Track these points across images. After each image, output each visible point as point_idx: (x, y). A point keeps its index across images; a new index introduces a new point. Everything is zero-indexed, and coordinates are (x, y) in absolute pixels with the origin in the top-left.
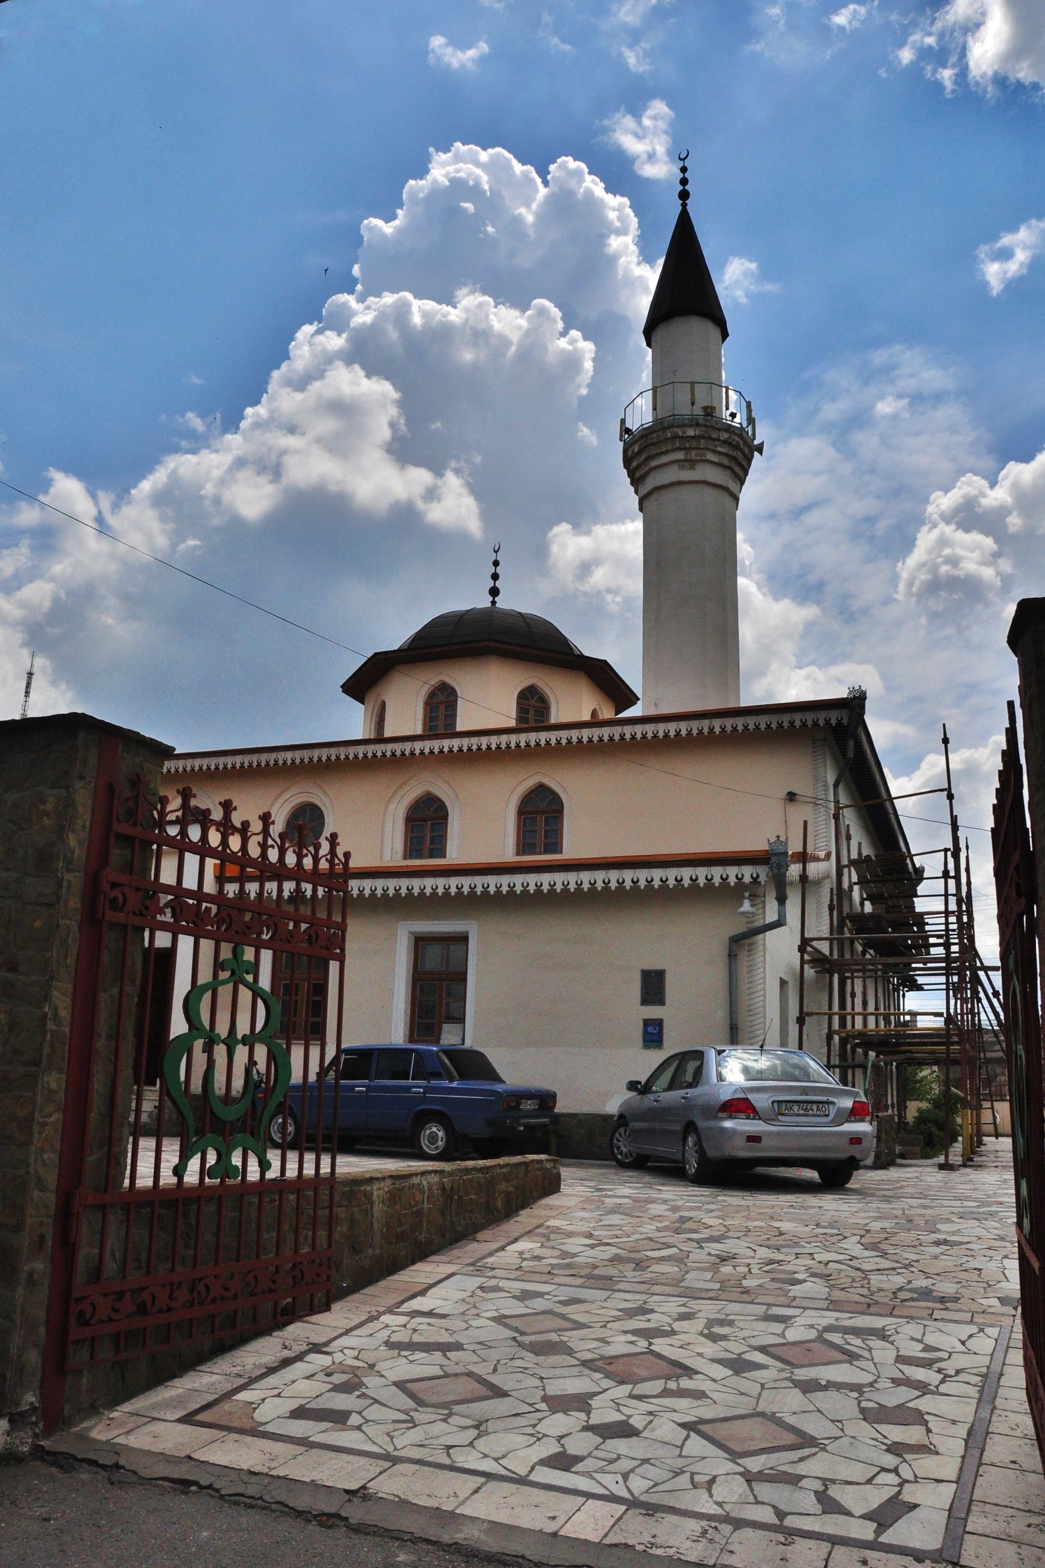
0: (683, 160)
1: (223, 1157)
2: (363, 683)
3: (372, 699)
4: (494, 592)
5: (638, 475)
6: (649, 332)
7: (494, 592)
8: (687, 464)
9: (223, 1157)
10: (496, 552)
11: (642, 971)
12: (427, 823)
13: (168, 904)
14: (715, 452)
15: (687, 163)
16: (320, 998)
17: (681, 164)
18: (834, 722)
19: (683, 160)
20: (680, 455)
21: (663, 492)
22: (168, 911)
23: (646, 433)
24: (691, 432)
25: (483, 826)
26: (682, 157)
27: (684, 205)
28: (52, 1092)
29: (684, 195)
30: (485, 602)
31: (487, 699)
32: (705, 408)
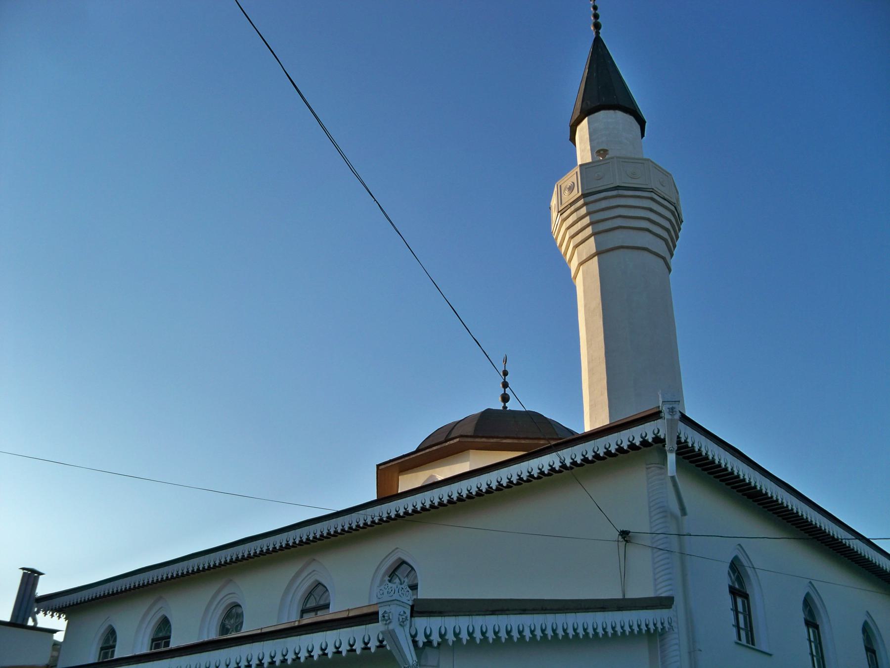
4: (505, 398)
7: (505, 398)
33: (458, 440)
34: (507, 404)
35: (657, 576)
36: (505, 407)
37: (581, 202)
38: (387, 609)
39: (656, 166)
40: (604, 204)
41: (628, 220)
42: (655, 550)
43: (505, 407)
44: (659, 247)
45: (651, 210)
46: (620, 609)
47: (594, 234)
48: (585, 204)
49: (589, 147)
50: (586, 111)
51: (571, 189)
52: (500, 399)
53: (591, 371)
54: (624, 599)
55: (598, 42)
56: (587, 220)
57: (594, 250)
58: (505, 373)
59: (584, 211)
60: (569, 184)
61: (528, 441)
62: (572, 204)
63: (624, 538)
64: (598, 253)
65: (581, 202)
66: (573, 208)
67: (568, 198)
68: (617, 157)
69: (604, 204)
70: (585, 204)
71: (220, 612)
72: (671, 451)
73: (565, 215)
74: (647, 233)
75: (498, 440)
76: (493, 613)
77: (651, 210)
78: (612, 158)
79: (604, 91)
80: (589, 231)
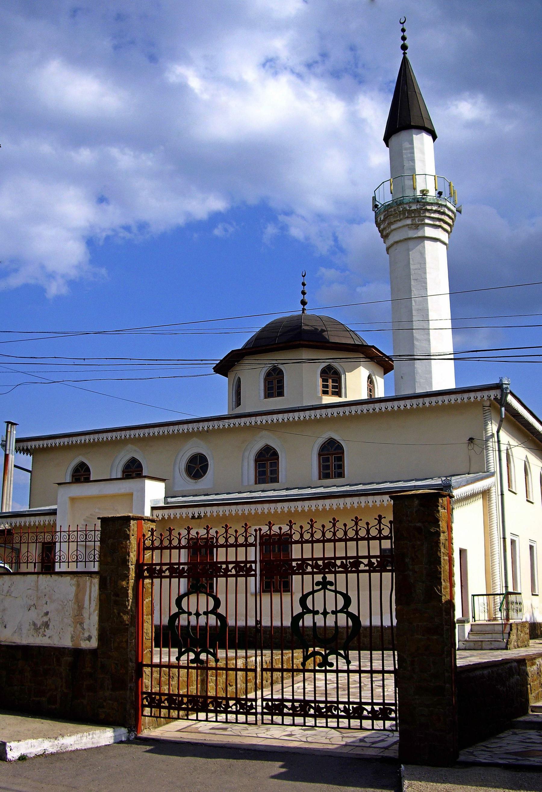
0: (403, 23)
1: (197, 655)
2: (224, 367)
3: (232, 374)
5: (385, 233)
6: (387, 139)
8: (413, 226)
9: (197, 655)
10: (304, 276)
13: (166, 699)
14: (430, 218)
15: (405, 26)
16: (274, 476)
17: (401, 27)
19: (403, 23)
20: (409, 222)
21: (399, 244)
22: (166, 702)
23: (388, 207)
24: (414, 207)
26: (402, 22)
27: (404, 54)
28: (133, 633)
29: (404, 47)
30: (296, 310)
32: (422, 191)
55: (405, 62)
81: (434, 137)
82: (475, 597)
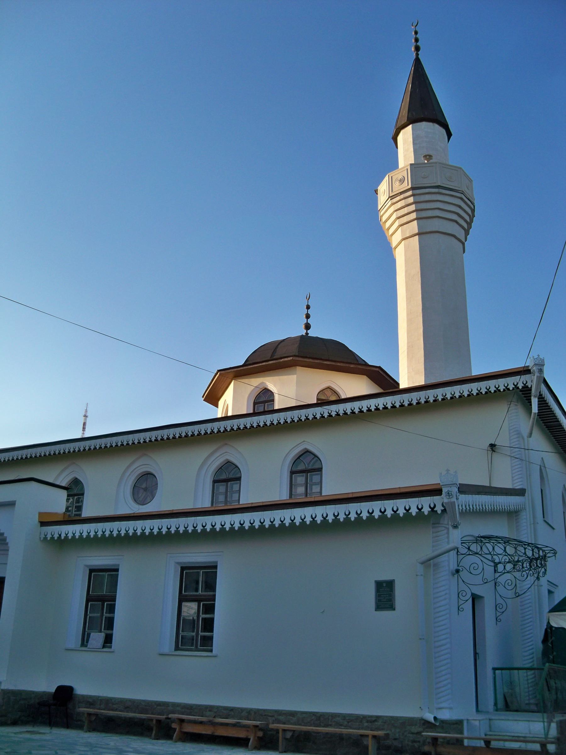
4: (308, 327)
7: (308, 327)
11: (394, 610)
12: (227, 477)
18: (520, 386)
25: (265, 473)
30: (304, 332)
31: (289, 389)
33: (291, 358)
34: (309, 331)
35: (514, 471)
36: (307, 334)
37: (410, 193)
38: (450, 489)
39: (465, 174)
40: (427, 197)
41: (446, 213)
42: (513, 458)
43: (307, 334)
44: (460, 234)
45: (460, 207)
46: (486, 493)
47: (417, 219)
48: (413, 195)
49: (412, 149)
50: (412, 121)
51: (402, 181)
52: (304, 326)
53: (410, 321)
54: (490, 487)
55: (418, 63)
56: (413, 207)
57: (416, 231)
58: (308, 307)
59: (411, 200)
60: (400, 177)
61: (342, 364)
62: (401, 193)
63: (492, 449)
64: (419, 234)
65: (410, 193)
66: (402, 196)
67: (398, 188)
68: (440, 163)
69: (427, 197)
70: (413, 195)
71: (133, 478)
72: (535, 396)
73: (395, 200)
74: (455, 224)
75: (321, 361)
76: (479, 493)
77: (460, 207)
78: (436, 163)
79: (423, 107)
80: (414, 216)
81: (449, 135)
82: (497, 671)
